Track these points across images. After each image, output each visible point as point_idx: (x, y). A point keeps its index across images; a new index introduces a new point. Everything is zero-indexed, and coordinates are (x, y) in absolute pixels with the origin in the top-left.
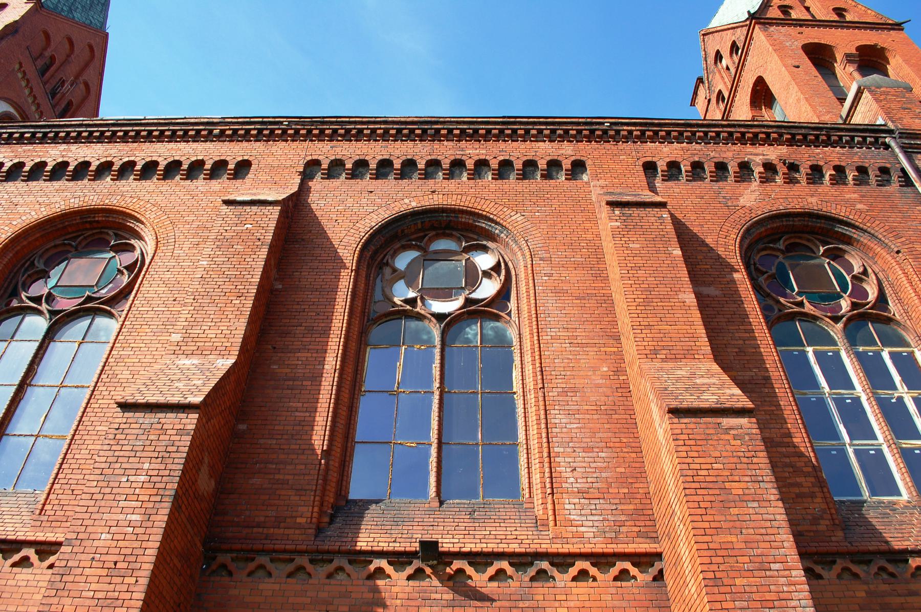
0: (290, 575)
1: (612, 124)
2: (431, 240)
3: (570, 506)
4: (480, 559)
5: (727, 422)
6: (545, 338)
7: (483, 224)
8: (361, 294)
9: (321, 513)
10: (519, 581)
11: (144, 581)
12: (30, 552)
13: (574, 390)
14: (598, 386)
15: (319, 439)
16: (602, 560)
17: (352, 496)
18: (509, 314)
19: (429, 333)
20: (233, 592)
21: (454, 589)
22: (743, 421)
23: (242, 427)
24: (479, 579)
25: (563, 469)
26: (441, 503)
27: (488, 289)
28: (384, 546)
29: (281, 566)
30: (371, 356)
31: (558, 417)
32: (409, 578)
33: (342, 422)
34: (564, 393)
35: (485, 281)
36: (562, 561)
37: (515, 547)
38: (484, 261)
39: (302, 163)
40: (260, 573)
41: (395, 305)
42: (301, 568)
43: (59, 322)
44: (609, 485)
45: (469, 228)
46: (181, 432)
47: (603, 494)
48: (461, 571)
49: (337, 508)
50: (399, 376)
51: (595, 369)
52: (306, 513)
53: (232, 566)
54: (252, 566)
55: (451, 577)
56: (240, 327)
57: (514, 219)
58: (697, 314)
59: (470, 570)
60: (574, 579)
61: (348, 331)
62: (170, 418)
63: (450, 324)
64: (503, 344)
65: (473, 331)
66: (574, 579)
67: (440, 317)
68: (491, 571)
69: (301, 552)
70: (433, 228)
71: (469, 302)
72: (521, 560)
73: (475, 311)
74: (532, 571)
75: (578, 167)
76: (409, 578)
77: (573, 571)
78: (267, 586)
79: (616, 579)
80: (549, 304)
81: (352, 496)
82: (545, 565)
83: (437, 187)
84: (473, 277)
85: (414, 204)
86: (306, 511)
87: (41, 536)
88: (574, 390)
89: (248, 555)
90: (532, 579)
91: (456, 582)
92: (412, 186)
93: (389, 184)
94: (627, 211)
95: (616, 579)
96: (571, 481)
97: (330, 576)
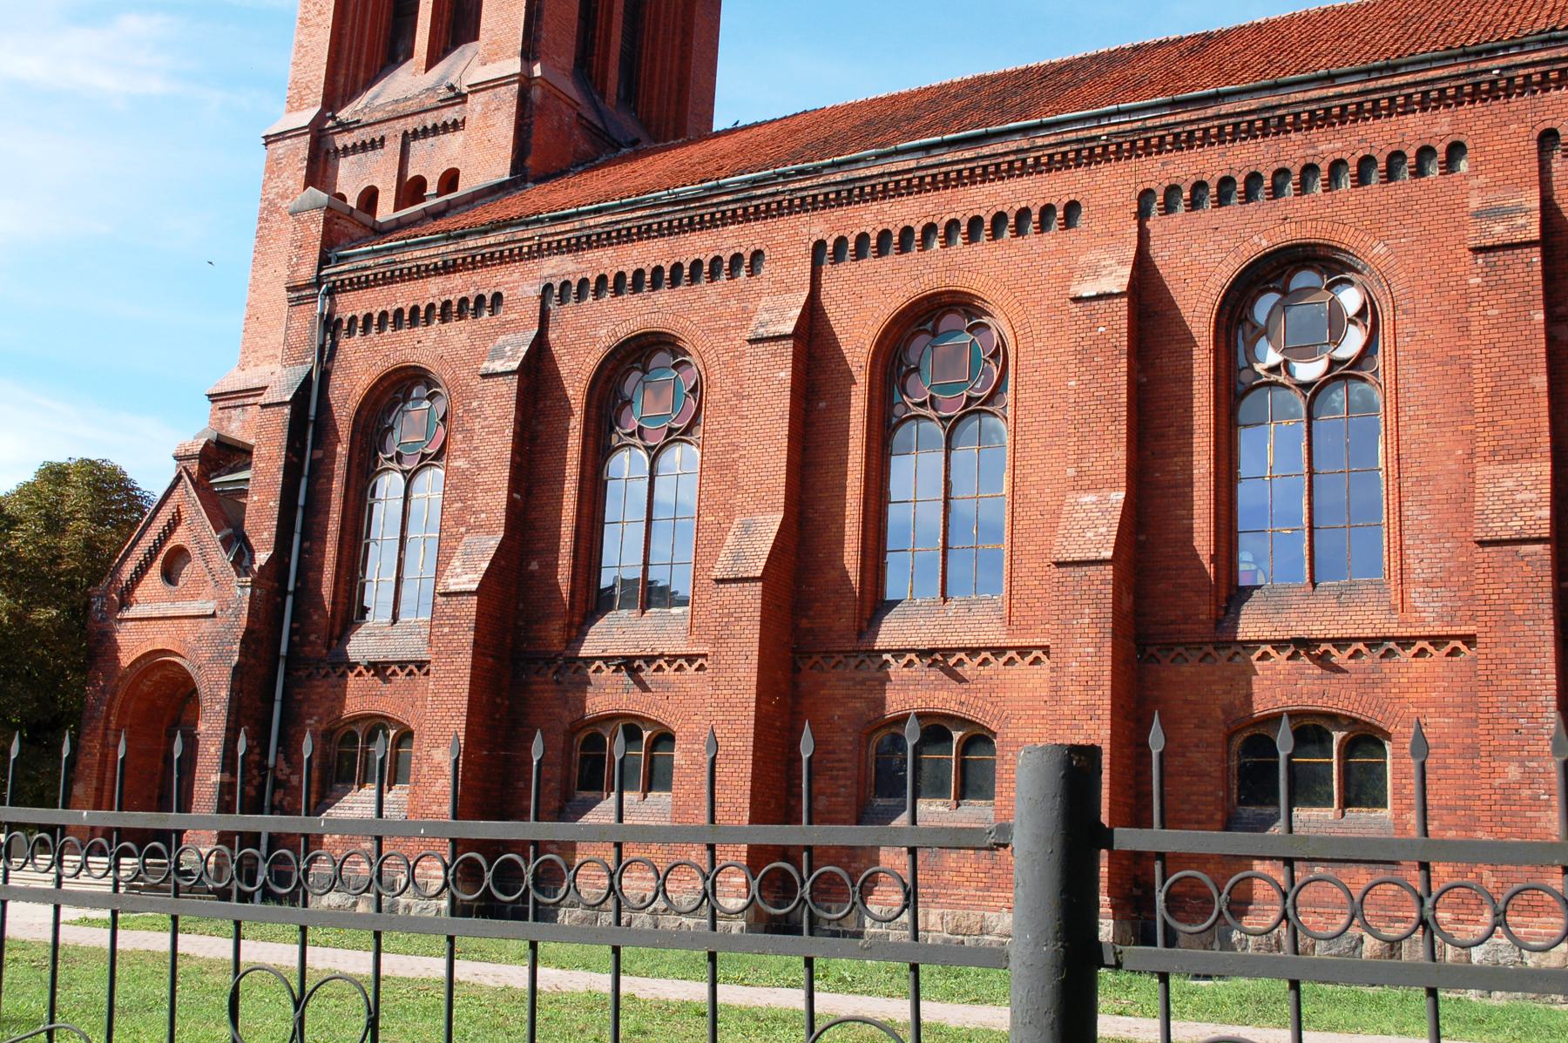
0: (1201, 660)
1: (1502, 69)
2: (1290, 277)
3: (1415, 595)
4: (1341, 643)
5: (1525, 549)
6: (1403, 419)
7: (1342, 257)
8: (1223, 374)
9: (1218, 606)
10: (1369, 659)
11: (1108, 693)
12: (1013, 653)
13: (1428, 479)
14: (1451, 472)
15: (1203, 541)
16: (1437, 641)
17: (1241, 583)
18: (1376, 373)
19: (1296, 404)
20: (1163, 675)
21: (1322, 667)
22: (1538, 548)
23: (1143, 538)
24: (1339, 657)
25: (1411, 561)
26: (1314, 586)
27: (1353, 342)
28: (1267, 635)
29: (1194, 652)
30: (1245, 437)
31: (1410, 509)
32: (1289, 658)
33: (1223, 522)
34: (1418, 482)
35: (1352, 328)
36: (1405, 642)
37: (1368, 633)
38: (1350, 299)
39: (1134, 196)
40: (1180, 659)
41: (1259, 376)
42: (1208, 654)
43: (952, 427)
44: (1451, 574)
45: (1329, 262)
46: (1103, 582)
47: (1445, 583)
48: (1327, 652)
49: (1229, 599)
50: (1270, 460)
51: (1449, 453)
52: (1205, 611)
53: (1159, 655)
54: (1173, 654)
55: (1319, 657)
56: (1121, 454)
57: (1376, 252)
58: (1545, 403)
59: (1334, 651)
60: (1415, 656)
61: (1216, 424)
62: (1091, 571)
63: (1314, 391)
64: (1369, 407)
65: (1338, 396)
66: (1415, 656)
67: (1304, 386)
68: (1350, 651)
69: (1206, 643)
70: (1291, 262)
71: (1333, 363)
72: (1373, 643)
73: (1341, 373)
74: (1382, 651)
75: (1456, 150)
76: (1289, 658)
77: (1415, 649)
78: (1187, 669)
79: (1448, 655)
80: (1409, 370)
81: (1241, 583)
82: (1392, 645)
83: (1289, 211)
84: (1336, 323)
85: (1264, 243)
86: (1205, 608)
87: (1017, 642)
88: (1428, 479)
89: (1169, 647)
90: (1382, 657)
91: (1323, 661)
92: (1260, 214)
93: (1234, 212)
94: (1492, 257)
95: (1448, 655)
96: (1418, 570)
97: (1230, 659)
